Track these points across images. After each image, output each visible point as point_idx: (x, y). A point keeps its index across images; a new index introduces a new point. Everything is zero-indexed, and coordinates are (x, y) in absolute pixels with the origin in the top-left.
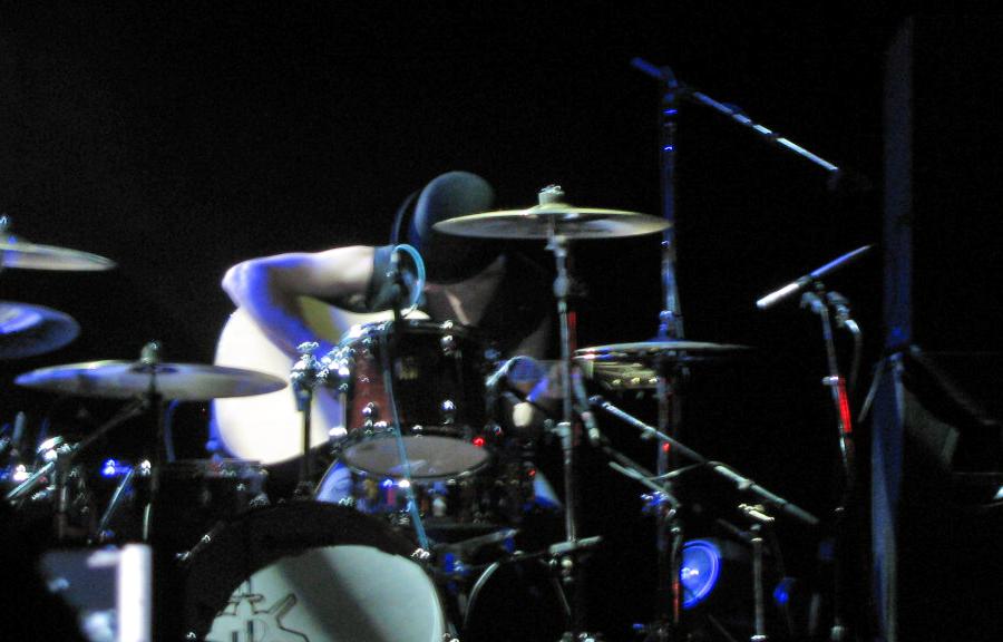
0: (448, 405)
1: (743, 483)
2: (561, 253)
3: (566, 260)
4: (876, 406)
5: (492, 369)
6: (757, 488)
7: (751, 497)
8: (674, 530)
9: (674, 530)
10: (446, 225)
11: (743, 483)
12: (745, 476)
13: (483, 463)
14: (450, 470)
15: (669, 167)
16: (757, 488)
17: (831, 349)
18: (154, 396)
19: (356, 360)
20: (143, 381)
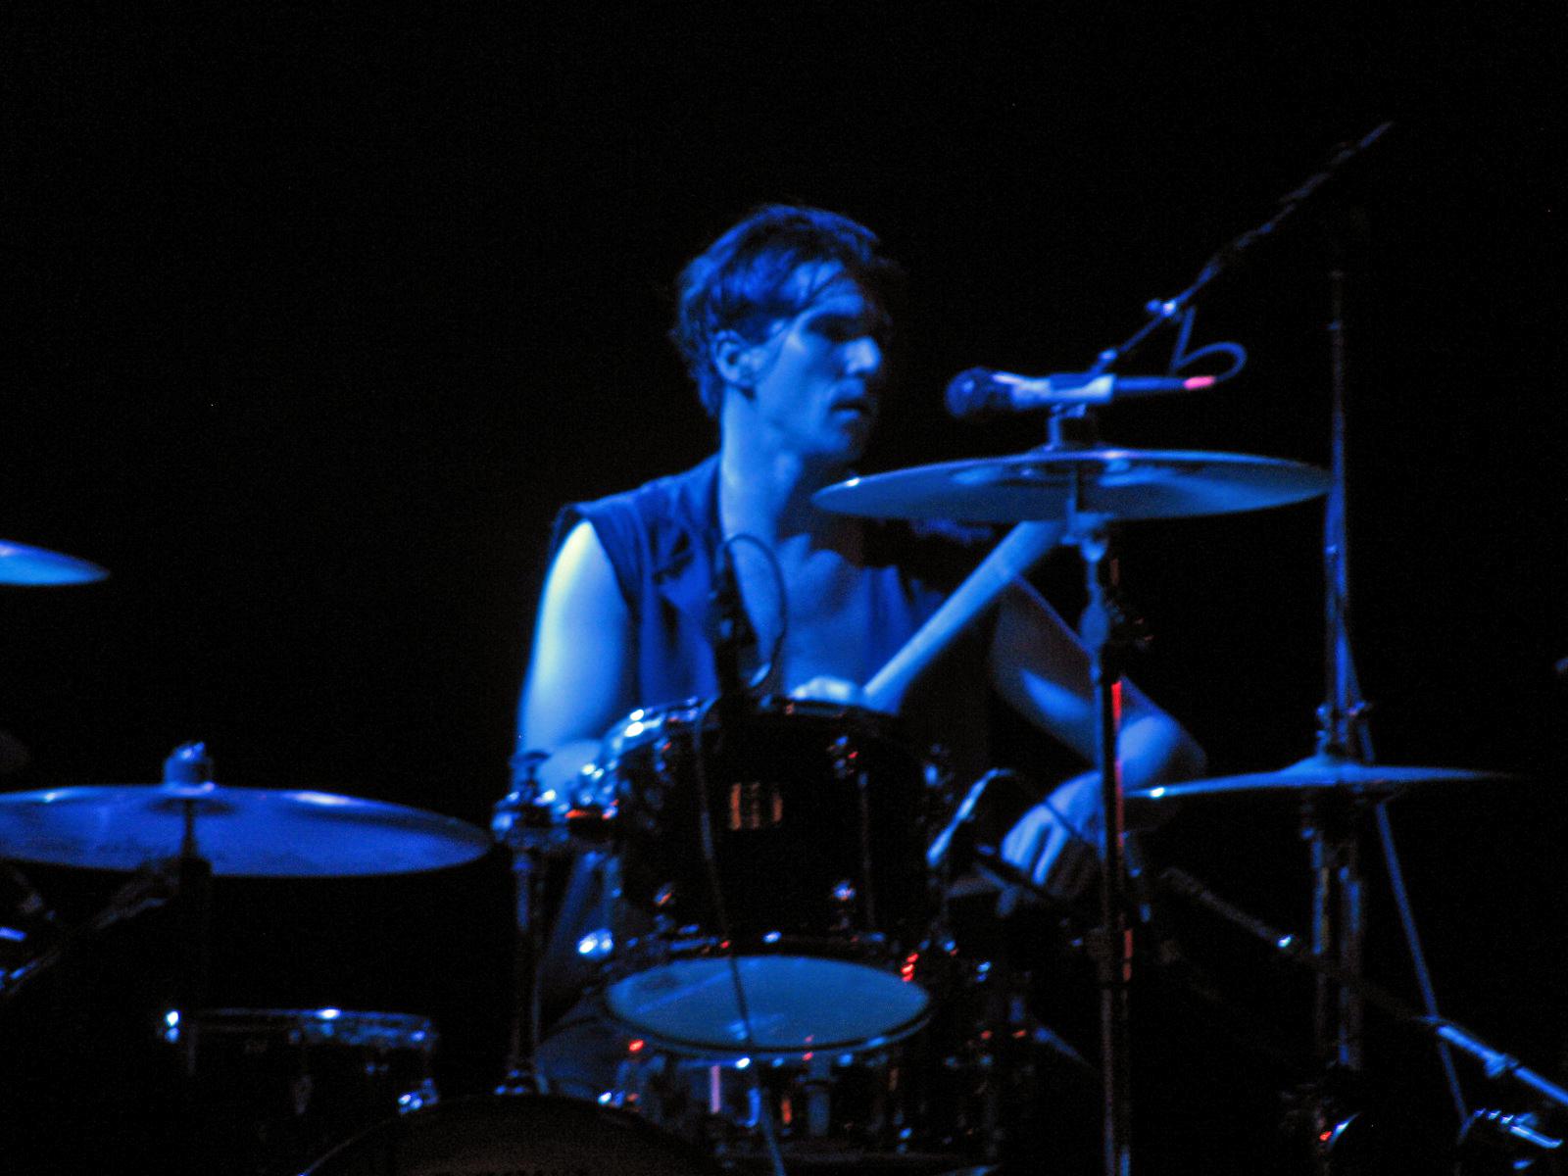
0: (844, 893)
1: (1494, 1061)
2: (1094, 554)
3: (1103, 565)
4: (634, 1174)
5: (942, 814)
6: (1525, 1075)
7: (1515, 1097)
8: (587, 946)
9: (587, 946)
10: (830, 496)
11: (1494, 1061)
12: (1499, 1048)
13: (920, 1017)
14: (847, 1035)
15: (1339, 341)
16: (1525, 1075)
17: (1107, 1037)
18: (191, 864)
19: (638, 790)
20: (167, 835)
